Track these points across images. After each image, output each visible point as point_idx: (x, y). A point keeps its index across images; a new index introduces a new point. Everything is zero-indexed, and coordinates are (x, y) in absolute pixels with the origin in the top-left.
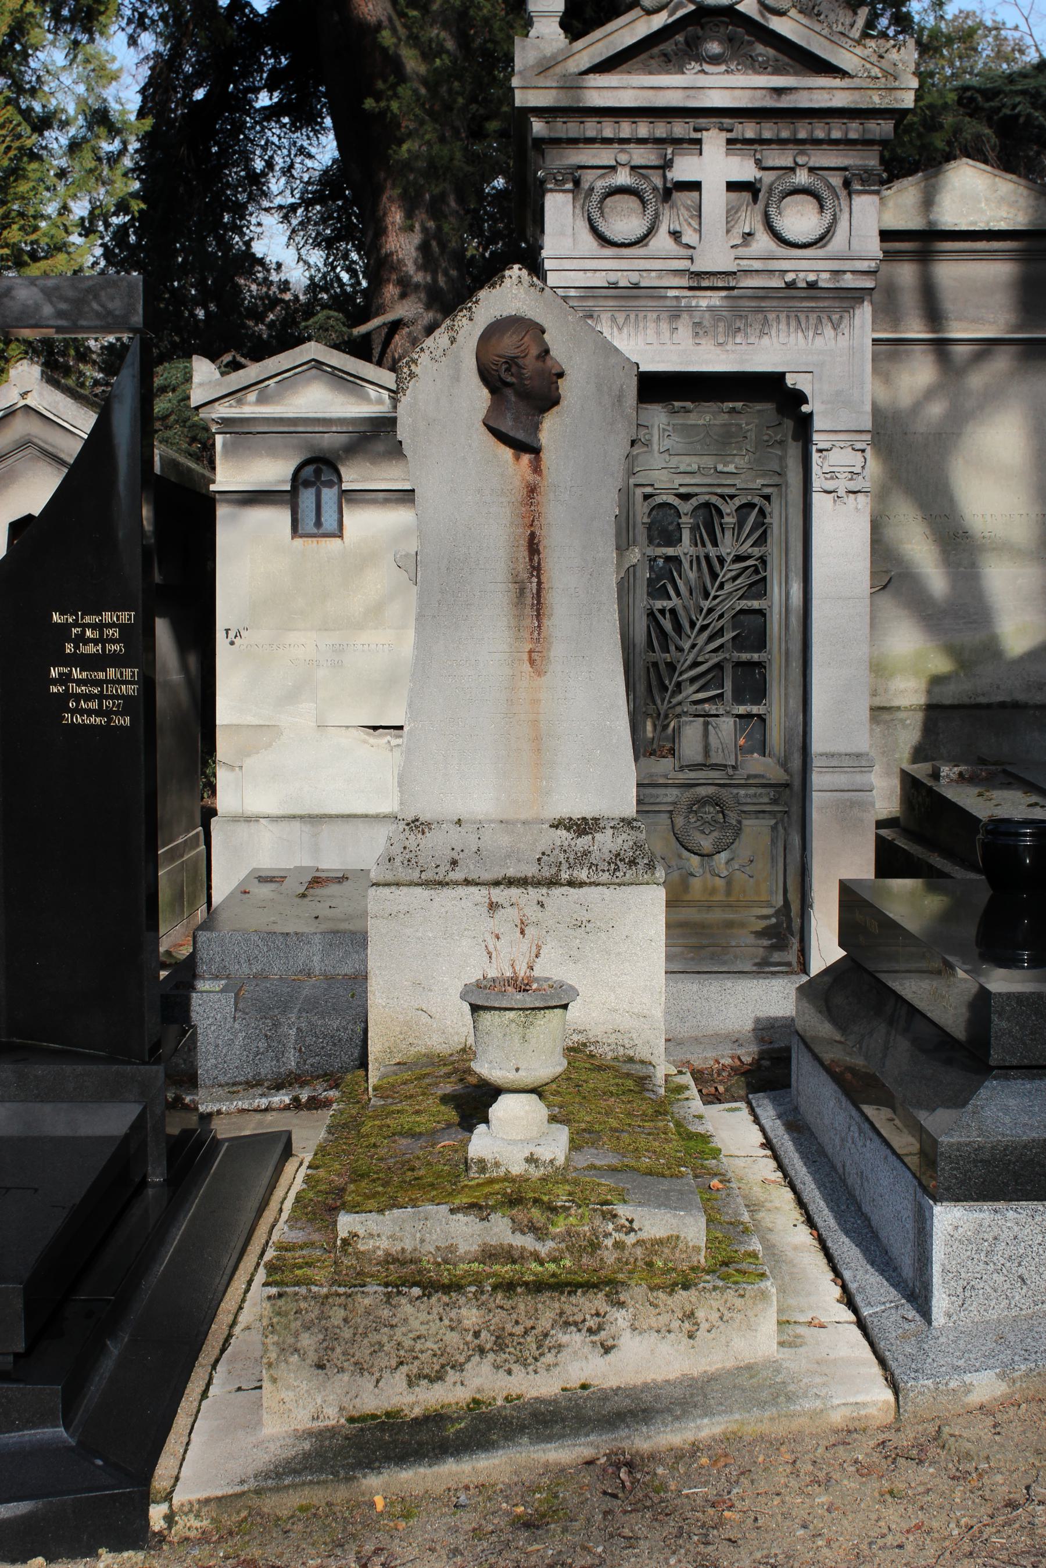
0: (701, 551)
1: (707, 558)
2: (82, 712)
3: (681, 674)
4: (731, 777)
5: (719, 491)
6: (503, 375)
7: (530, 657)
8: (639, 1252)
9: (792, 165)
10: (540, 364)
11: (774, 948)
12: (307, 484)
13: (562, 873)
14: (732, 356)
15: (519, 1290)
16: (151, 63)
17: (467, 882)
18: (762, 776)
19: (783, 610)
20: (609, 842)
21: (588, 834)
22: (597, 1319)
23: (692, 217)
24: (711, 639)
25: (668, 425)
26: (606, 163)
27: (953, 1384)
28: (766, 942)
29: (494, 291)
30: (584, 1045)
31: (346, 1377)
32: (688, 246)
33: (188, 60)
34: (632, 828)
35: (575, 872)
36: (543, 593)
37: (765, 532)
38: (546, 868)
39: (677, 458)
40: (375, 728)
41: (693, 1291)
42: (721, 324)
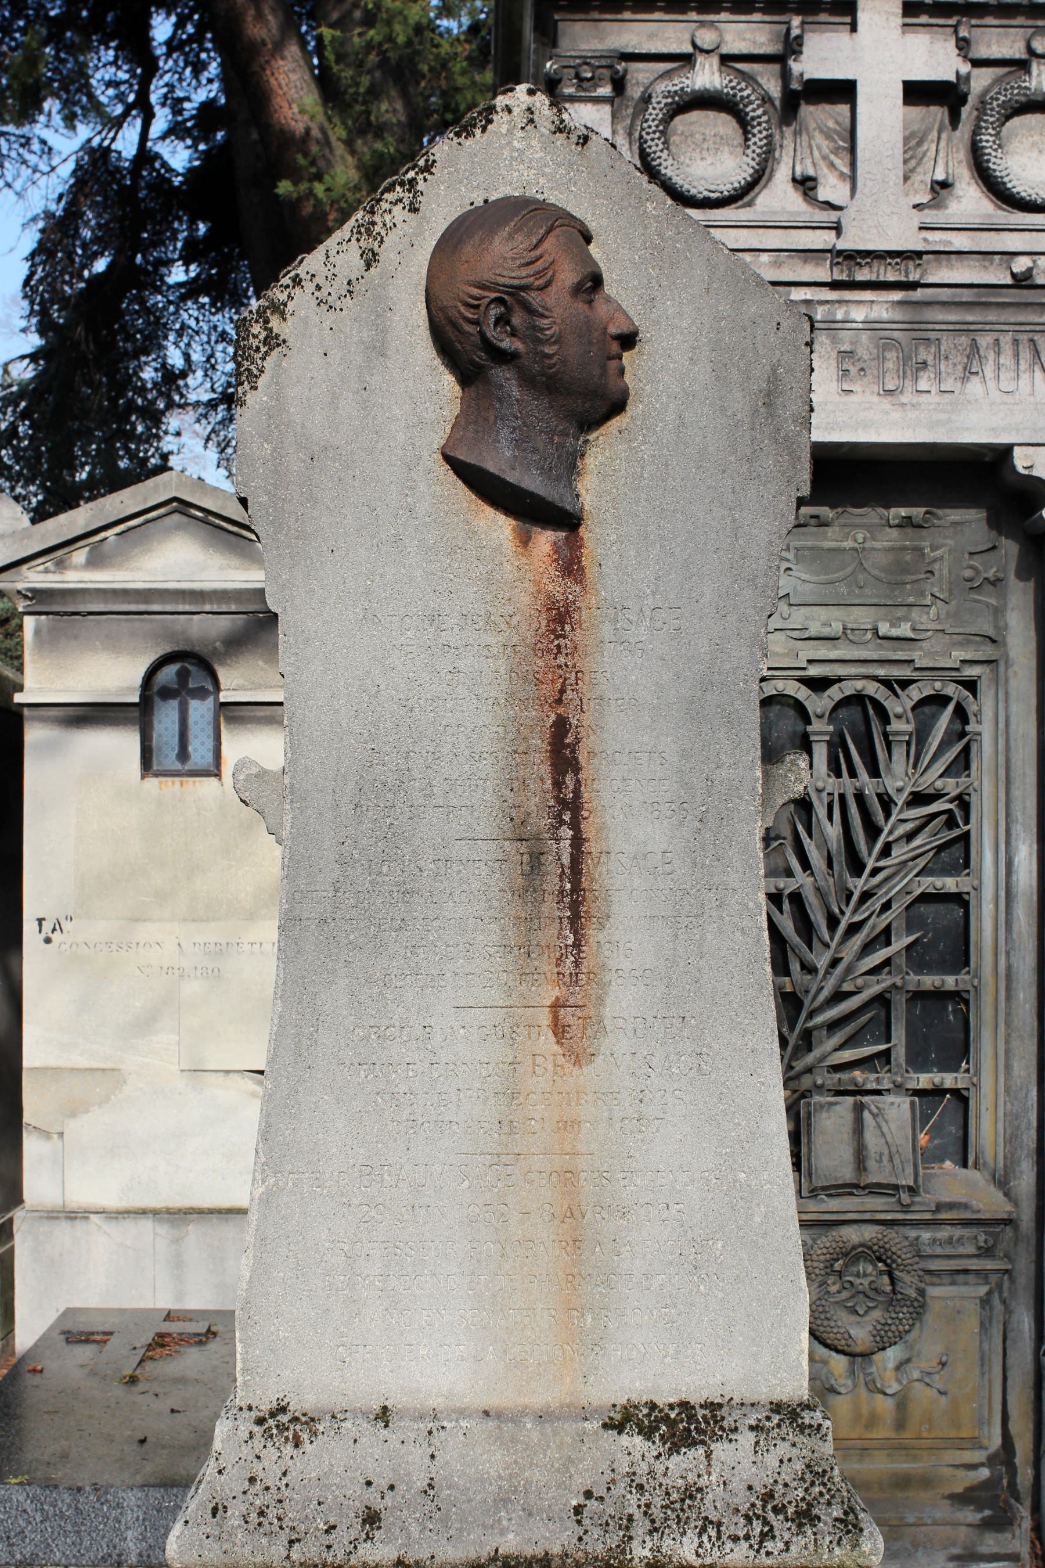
0: (847, 784)
1: (860, 797)
3: (811, 1015)
4: (906, 1208)
5: (881, 672)
6: (491, 333)
7: (556, 1019)
9: (1024, 56)
10: (581, 306)
11: (987, 1525)
12: (166, 694)
13: (635, 1544)
14: (912, 415)
16: (41, 224)
18: (966, 1206)
19: (1002, 894)
20: (746, 1463)
21: (694, 1444)
23: (836, 151)
24: (867, 948)
25: (788, 549)
26: (674, 48)
28: (971, 1515)
29: (469, 142)
33: (87, 224)
34: (802, 1428)
35: (667, 1542)
36: (588, 864)
37: (966, 750)
38: (596, 1532)
39: (803, 609)
42: (891, 355)
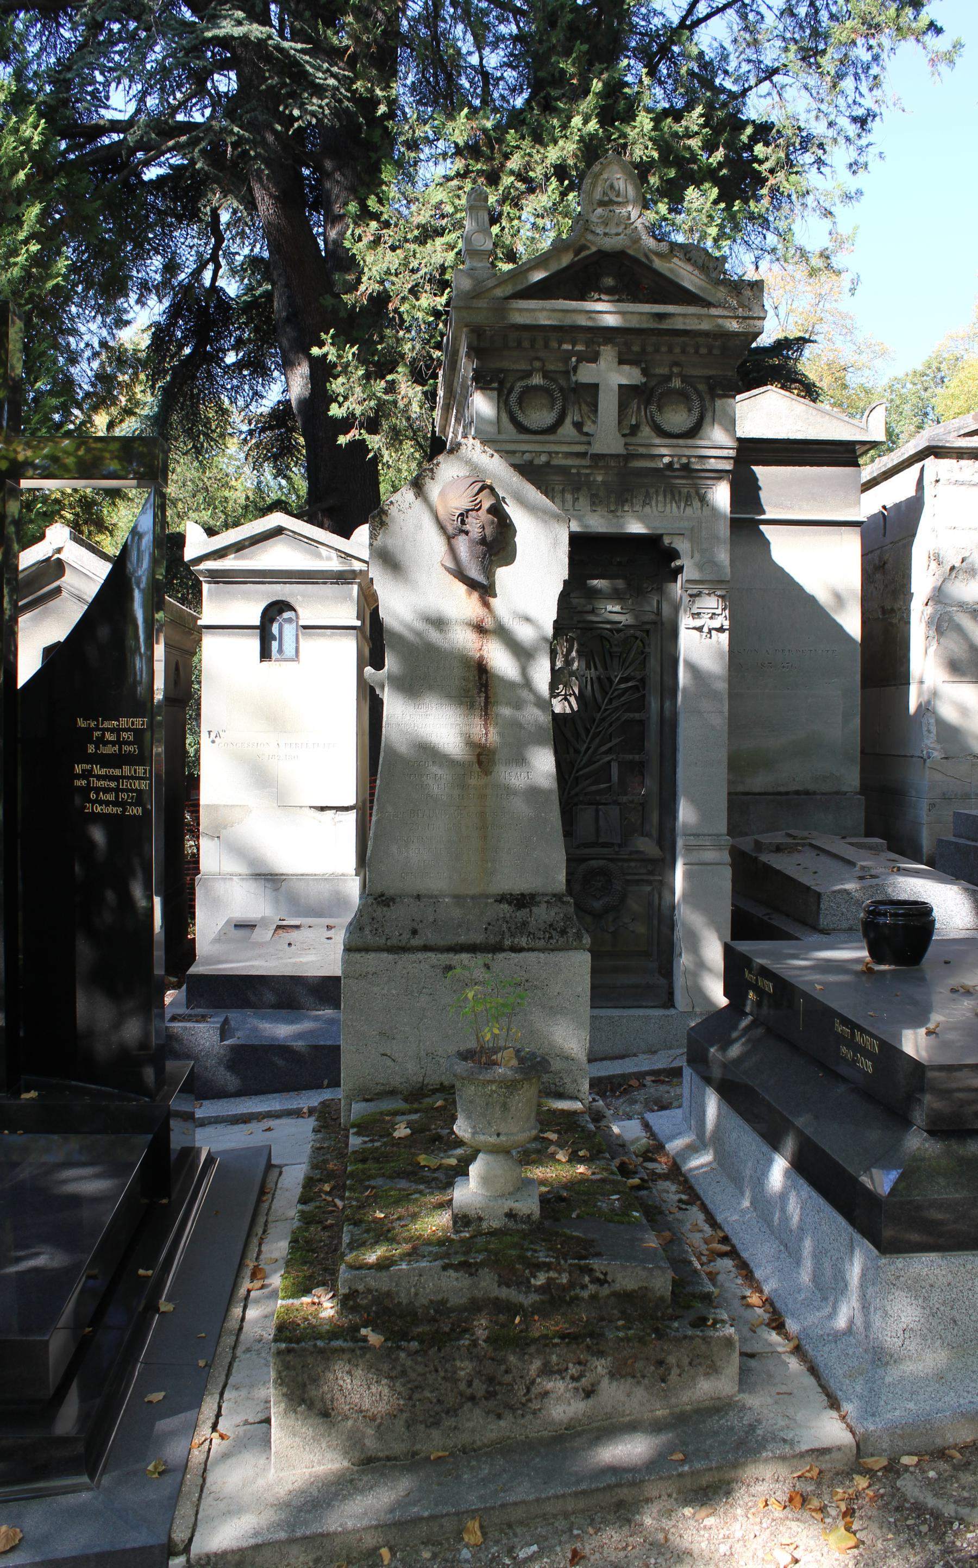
2: (101, 803)
17: (426, 948)
22: (579, 1368)
32: (587, 434)
40: (323, 809)
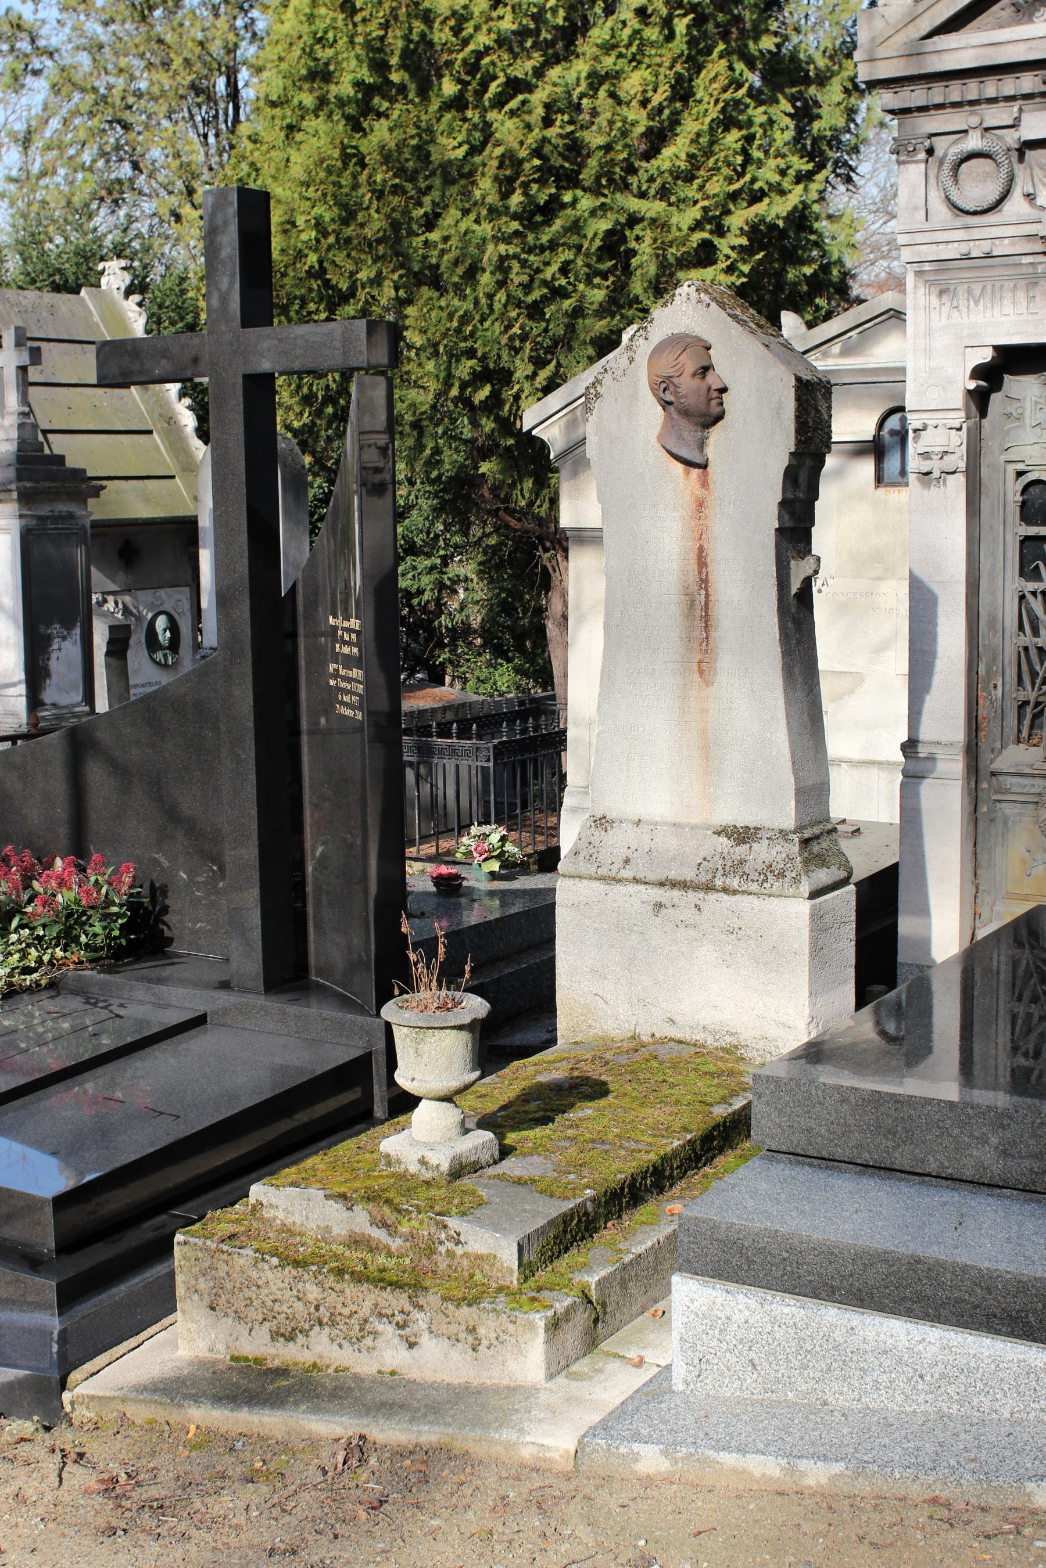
8: (465, 1262)
15: (347, 1277)
17: (636, 881)
27: (623, 1450)
30: (736, 1047)
31: (230, 1321)
36: (711, 605)
41: (474, 1309)
